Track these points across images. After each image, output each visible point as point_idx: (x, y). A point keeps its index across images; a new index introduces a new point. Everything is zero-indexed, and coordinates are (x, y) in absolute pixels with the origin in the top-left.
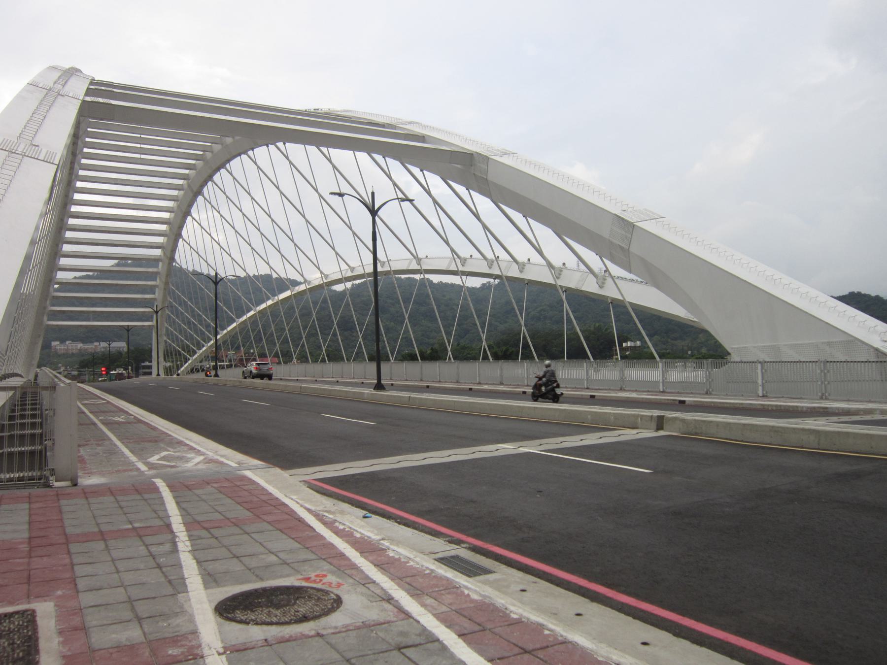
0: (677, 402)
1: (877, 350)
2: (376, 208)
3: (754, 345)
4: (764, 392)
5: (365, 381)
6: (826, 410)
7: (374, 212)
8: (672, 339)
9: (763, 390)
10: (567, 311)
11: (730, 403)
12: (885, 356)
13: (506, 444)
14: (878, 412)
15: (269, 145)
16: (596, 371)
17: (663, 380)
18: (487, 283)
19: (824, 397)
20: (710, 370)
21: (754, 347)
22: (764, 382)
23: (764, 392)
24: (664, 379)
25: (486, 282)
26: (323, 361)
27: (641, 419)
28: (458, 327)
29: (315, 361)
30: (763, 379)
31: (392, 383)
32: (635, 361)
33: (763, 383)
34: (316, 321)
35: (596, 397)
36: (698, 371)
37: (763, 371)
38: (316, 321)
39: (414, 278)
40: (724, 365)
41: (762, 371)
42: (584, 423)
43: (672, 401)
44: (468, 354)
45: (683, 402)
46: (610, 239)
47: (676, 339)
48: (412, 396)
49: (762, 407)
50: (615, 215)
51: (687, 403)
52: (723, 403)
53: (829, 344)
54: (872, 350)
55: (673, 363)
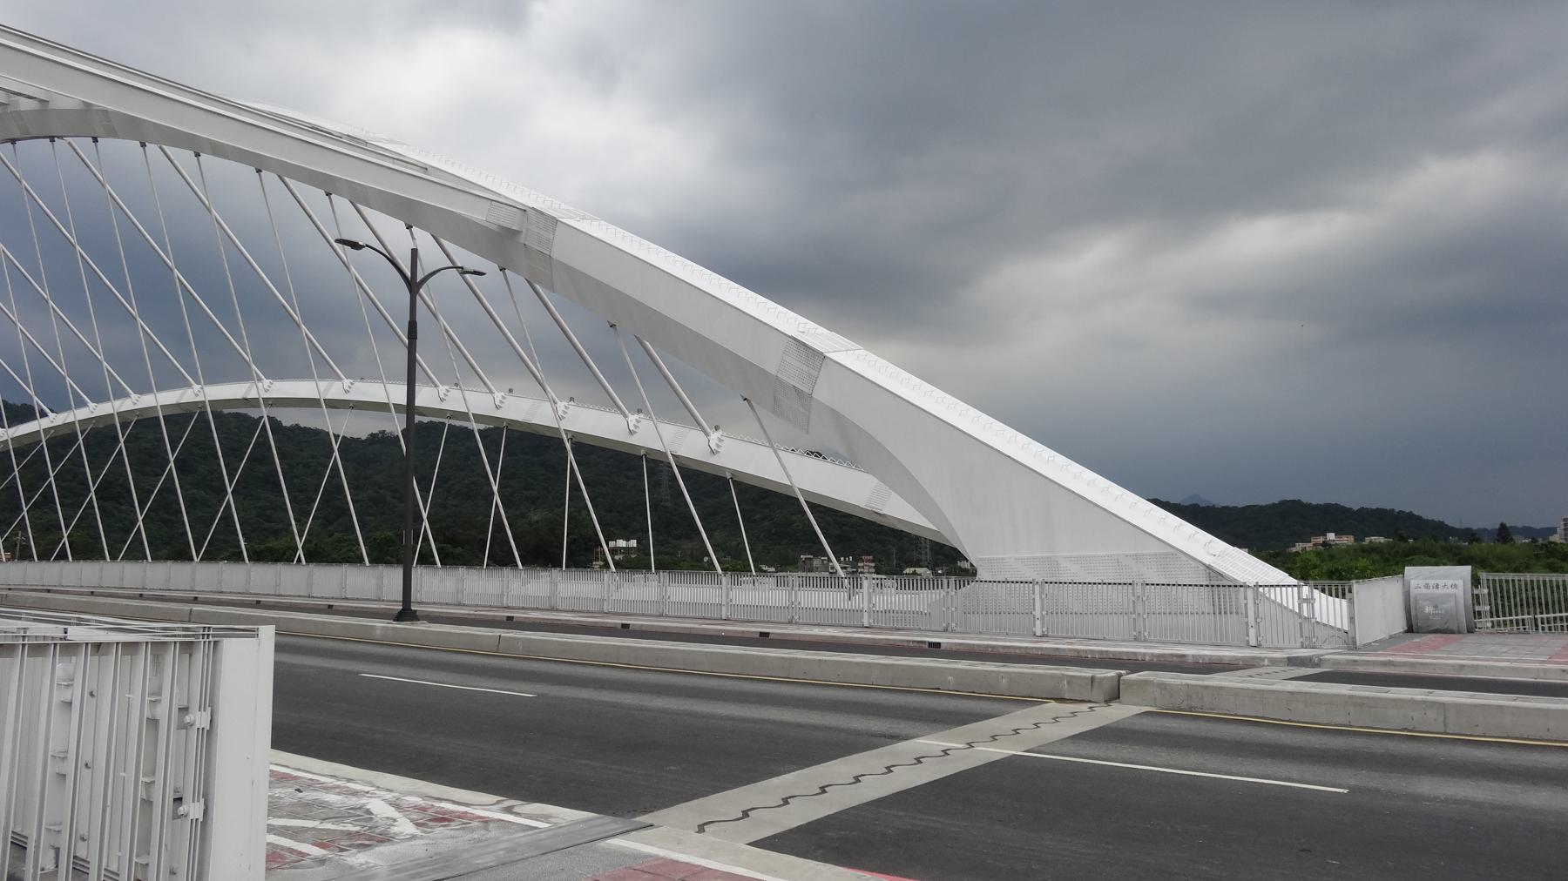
0: (926, 646)
1: (1209, 567)
2: (420, 277)
3: (1016, 556)
4: (1045, 630)
5: (145, 593)
6: (1182, 660)
7: (413, 285)
8: (674, 538)
9: (1043, 627)
10: (495, 481)
11: (1020, 648)
12: (1220, 577)
13: (1004, 756)
14: (1266, 662)
15: (56, 139)
16: (524, 584)
17: (870, 608)
18: (380, 432)
19: (950, 629)
20: (797, 589)
21: (1017, 559)
22: (1044, 613)
23: (1045, 630)
24: (871, 606)
25: (377, 432)
26: (62, 556)
27: (1068, 683)
28: (293, 504)
29: (44, 556)
30: (1042, 609)
31: (509, 615)
32: (627, 571)
33: (1043, 616)
34: (18, 480)
35: (771, 637)
36: (903, 594)
37: (1043, 596)
38: (18, 480)
39: (246, 415)
40: (964, 586)
41: (1041, 596)
42: (939, 689)
43: (915, 644)
44: (350, 551)
45: (938, 645)
46: (779, 375)
47: (679, 538)
48: (503, 635)
49: (1076, 654)
50: (792, 337)
51: (943, 647)
52: (1009, 647)
53: (1137, 557)
54: (1202, 568)
55: (837, 580)
